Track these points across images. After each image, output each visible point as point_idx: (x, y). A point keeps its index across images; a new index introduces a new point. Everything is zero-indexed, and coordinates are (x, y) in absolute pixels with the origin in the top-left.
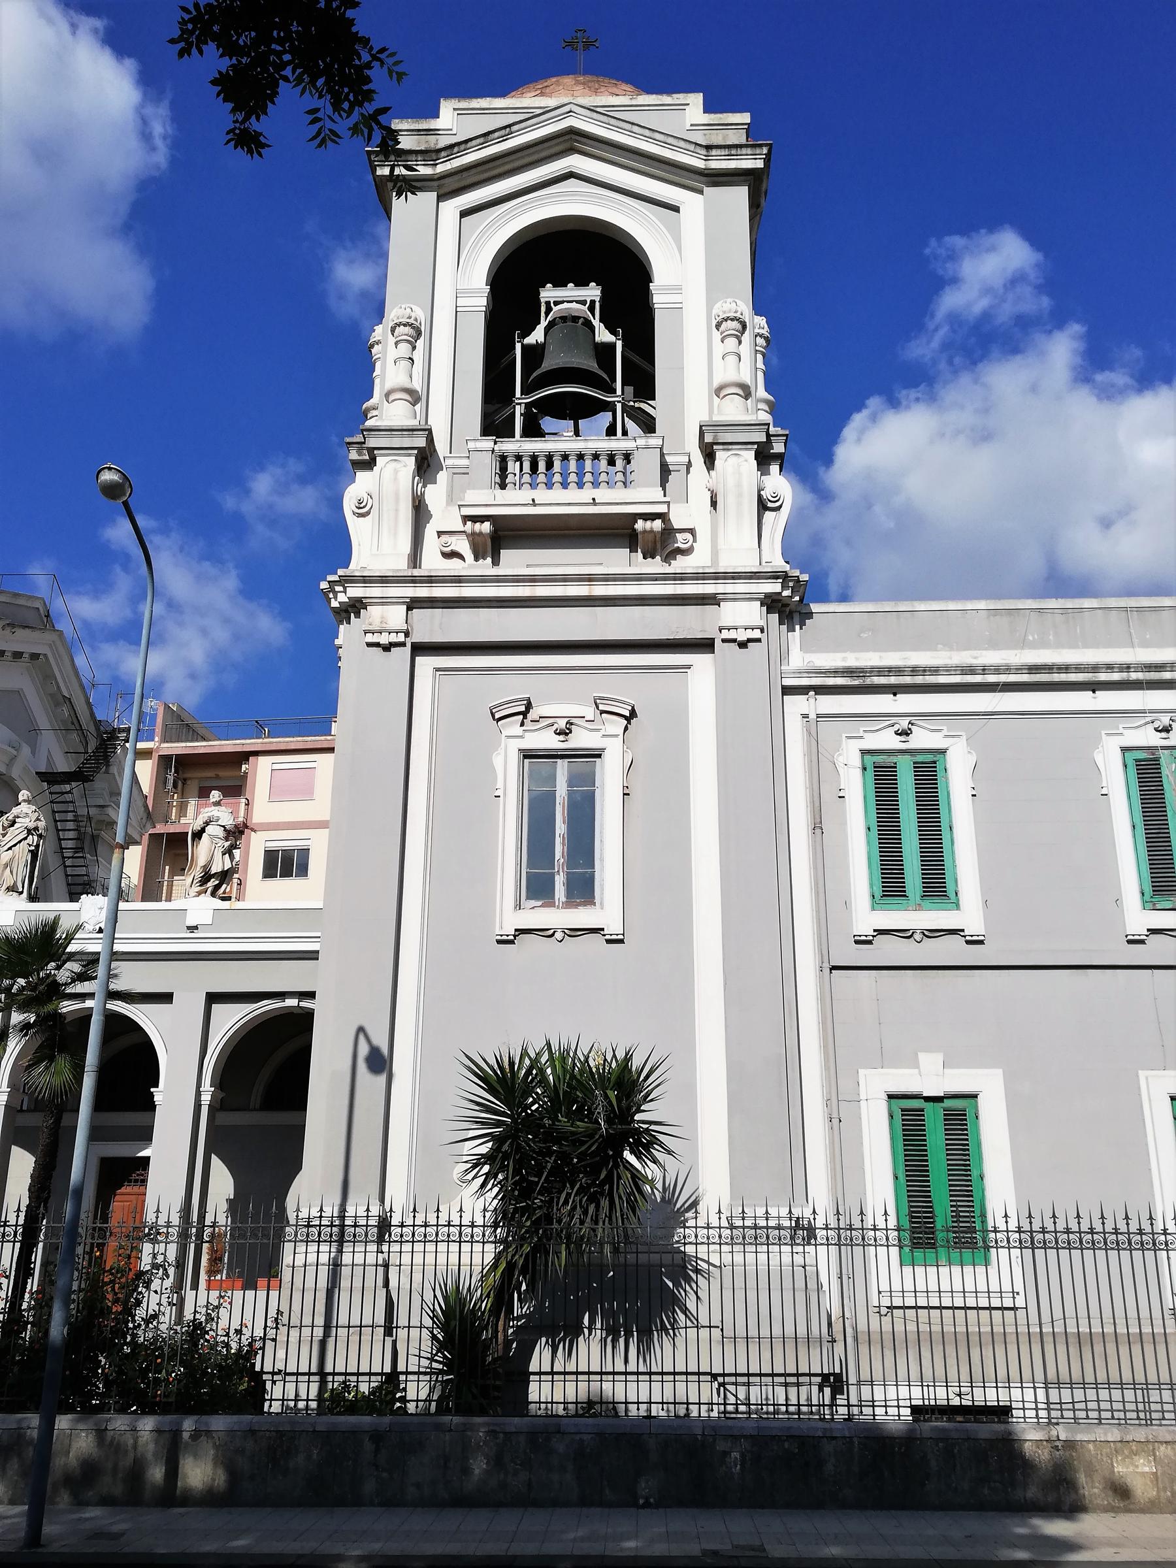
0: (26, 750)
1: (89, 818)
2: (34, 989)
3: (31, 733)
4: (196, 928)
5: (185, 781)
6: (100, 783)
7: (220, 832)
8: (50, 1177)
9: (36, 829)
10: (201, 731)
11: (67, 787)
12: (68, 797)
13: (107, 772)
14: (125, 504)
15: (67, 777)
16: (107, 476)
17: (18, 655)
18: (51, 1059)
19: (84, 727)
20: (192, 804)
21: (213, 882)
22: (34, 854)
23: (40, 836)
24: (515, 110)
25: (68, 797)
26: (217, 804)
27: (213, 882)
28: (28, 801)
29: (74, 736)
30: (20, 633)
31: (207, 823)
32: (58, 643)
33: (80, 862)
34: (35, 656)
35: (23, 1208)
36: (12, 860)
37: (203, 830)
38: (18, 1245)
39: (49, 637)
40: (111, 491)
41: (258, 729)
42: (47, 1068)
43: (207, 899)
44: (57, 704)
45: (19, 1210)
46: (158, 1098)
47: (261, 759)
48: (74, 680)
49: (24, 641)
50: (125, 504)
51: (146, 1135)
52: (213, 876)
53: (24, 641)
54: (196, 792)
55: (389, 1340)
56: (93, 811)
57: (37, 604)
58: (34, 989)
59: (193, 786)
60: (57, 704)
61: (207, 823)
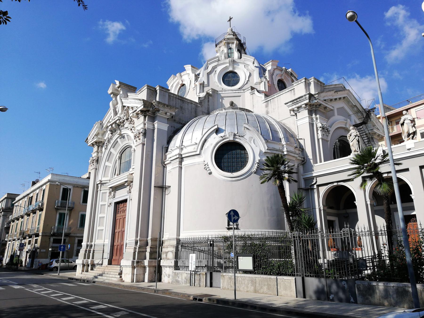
0: (349, 120)
1: (370, 133)
2: (370, 166)
3: (349, 116)
4: (410, 149)
5: (391, 122)
6: (369, 124)
7: (410, 122)
8: (391, 217)
9: (357, 135)
10: (392, 108)
11: (361, 127)
12: (363, 129)
13: (370, 121)
14: (356, 21)
15: (361, 124)
16: (349, 15)
17: (340, 98)
18: (381, 184)
19: (361, 111)
20: (395, 127)
21: (411, 136)
22: (358, 141)
23: (359, 137)
25: (363, 129)
26: (406, 114)
27: (411, 136)
28: (353, 129)
29: (359, 114)
30: (339, 93)
31: (404, 120)
32: (349, 93)
33: (370, 144)
34: (344, 98)
35: (385, 226)
36: (353, 144)
37: (404, 123)
38: (387, 236)
39: (346, 92)
40: (351, 18)
41: (408, 102)
42: (380, 187)
43: (411, 140)
44: (353, 108)
45: (384, 227)
46: (413, 197)
47: (411, 110)
48: (355, 100)
49: (341, 95)
50: (356, 21)
51: (413, 209)
52: (411, 134)
53: (341, 95)
54: (395, 124)
55: (99, 277)
56: (370, 131)
57: (341, 86)
58: (370, 166)
59: (394, 123)
60: (353, 108)
61: (404, 120)
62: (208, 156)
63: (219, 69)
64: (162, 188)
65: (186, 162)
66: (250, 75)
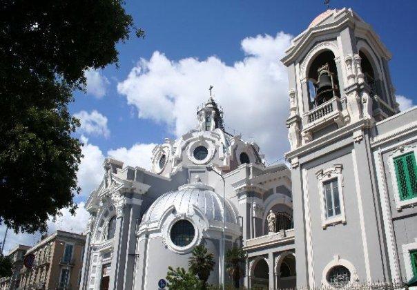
24: (300, 38)
62: (165, 234)
63: (191, 144)
64: (133, 256)
65: (151, 236)
66: (216, 151)
